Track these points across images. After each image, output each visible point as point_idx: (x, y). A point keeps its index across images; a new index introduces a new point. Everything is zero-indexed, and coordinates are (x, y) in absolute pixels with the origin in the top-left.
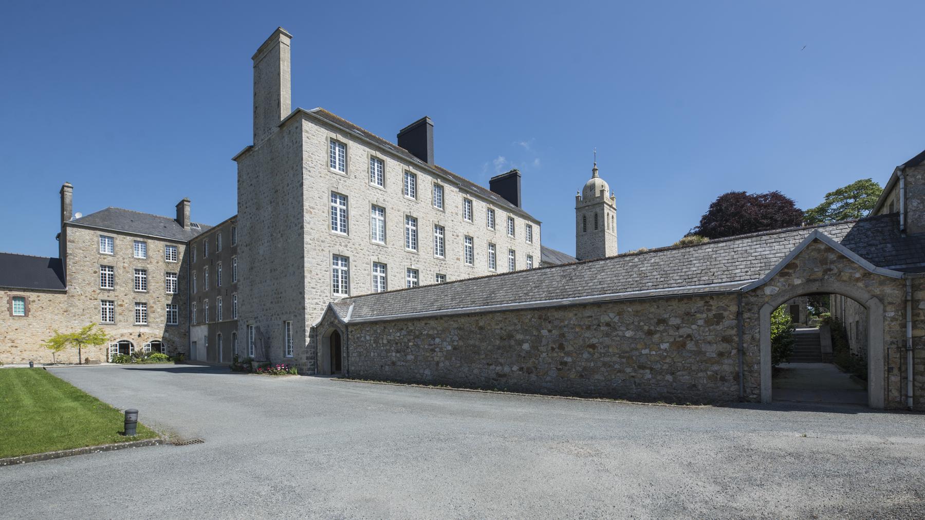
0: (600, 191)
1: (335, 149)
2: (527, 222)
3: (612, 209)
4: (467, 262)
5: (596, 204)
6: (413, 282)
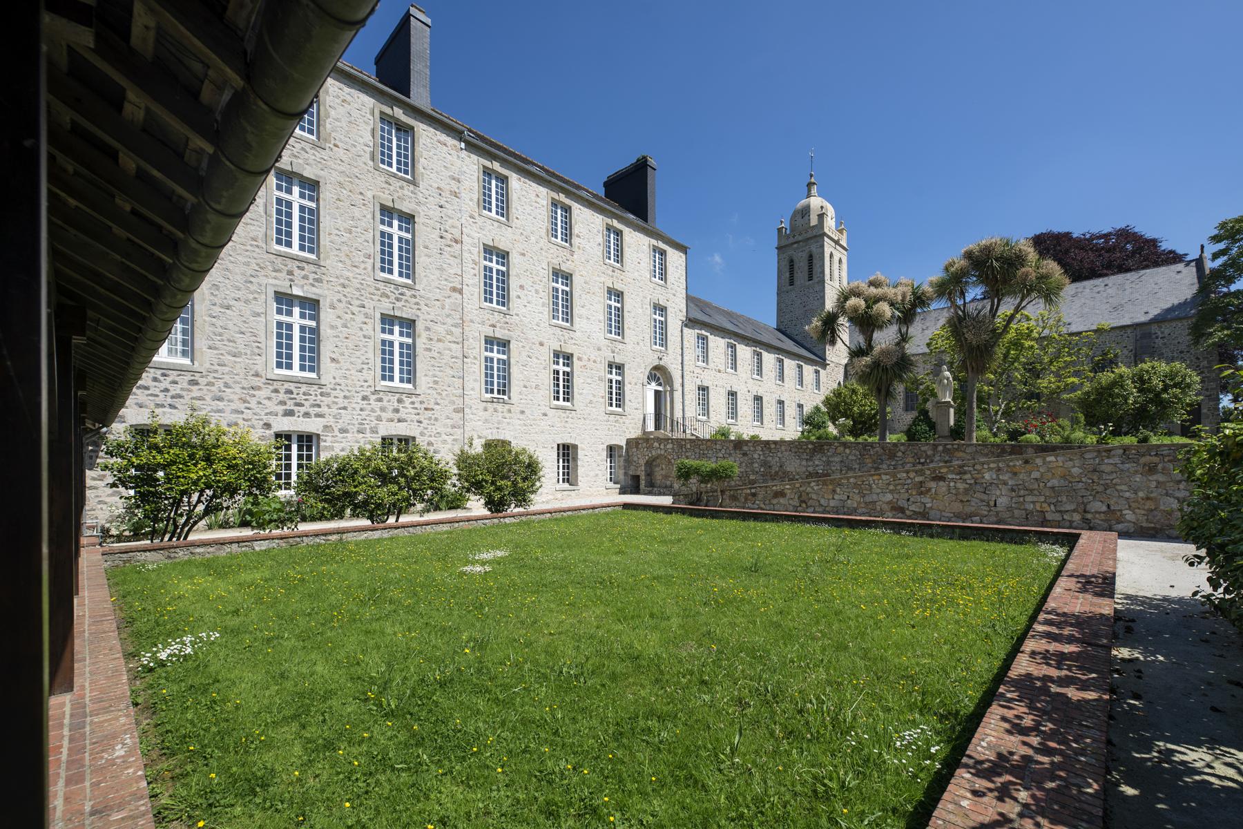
0: (818, 215)
1: (490, 183)
2: (654, 242)
3: (838, 247)
4: (656, 344)
5: (811, 238)
6: (564, 372)
